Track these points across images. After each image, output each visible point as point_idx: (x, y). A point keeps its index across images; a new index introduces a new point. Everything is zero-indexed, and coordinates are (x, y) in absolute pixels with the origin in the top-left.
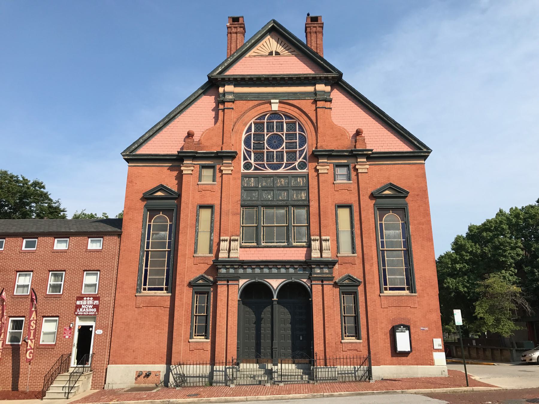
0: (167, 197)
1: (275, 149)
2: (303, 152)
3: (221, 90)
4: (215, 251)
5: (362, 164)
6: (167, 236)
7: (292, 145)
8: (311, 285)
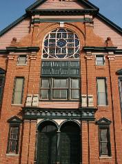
3: (33, 17)
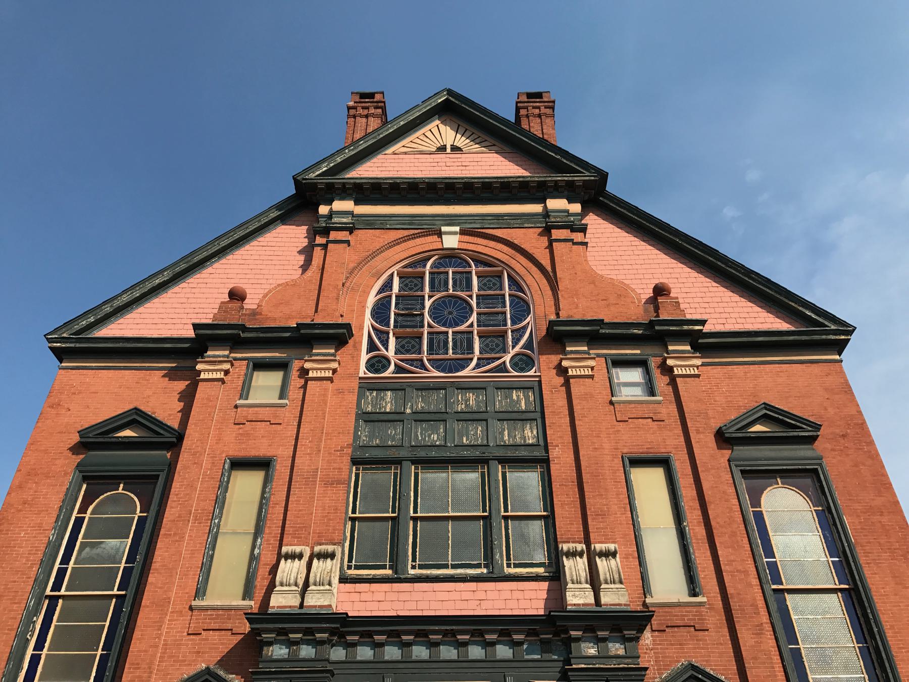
0: (145, 440)
1: (451, 326)
2: (524, 333)
3: (323, 210)
4: (259, 594)
5: (681, 356)
7: (494, 318)
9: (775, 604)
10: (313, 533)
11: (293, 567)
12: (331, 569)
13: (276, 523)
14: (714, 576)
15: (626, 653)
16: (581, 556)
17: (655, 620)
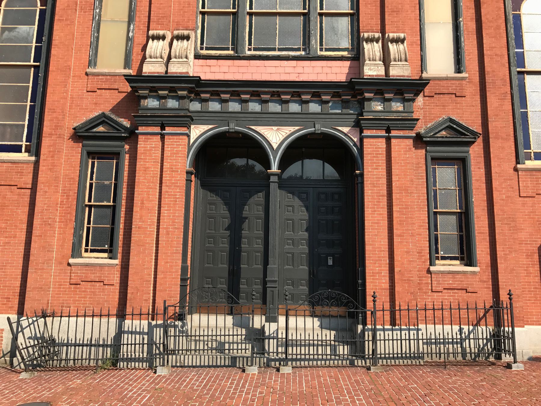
6: (33, 35)
8: (361, 140)
9: (517, 81)
10: (173, 22)
11: (158, 45)
12: (187, 47)
13: (143, 14)
14: (477, 59)
15: (404, 109)
16: (377, 41)
17: (427, 89)
